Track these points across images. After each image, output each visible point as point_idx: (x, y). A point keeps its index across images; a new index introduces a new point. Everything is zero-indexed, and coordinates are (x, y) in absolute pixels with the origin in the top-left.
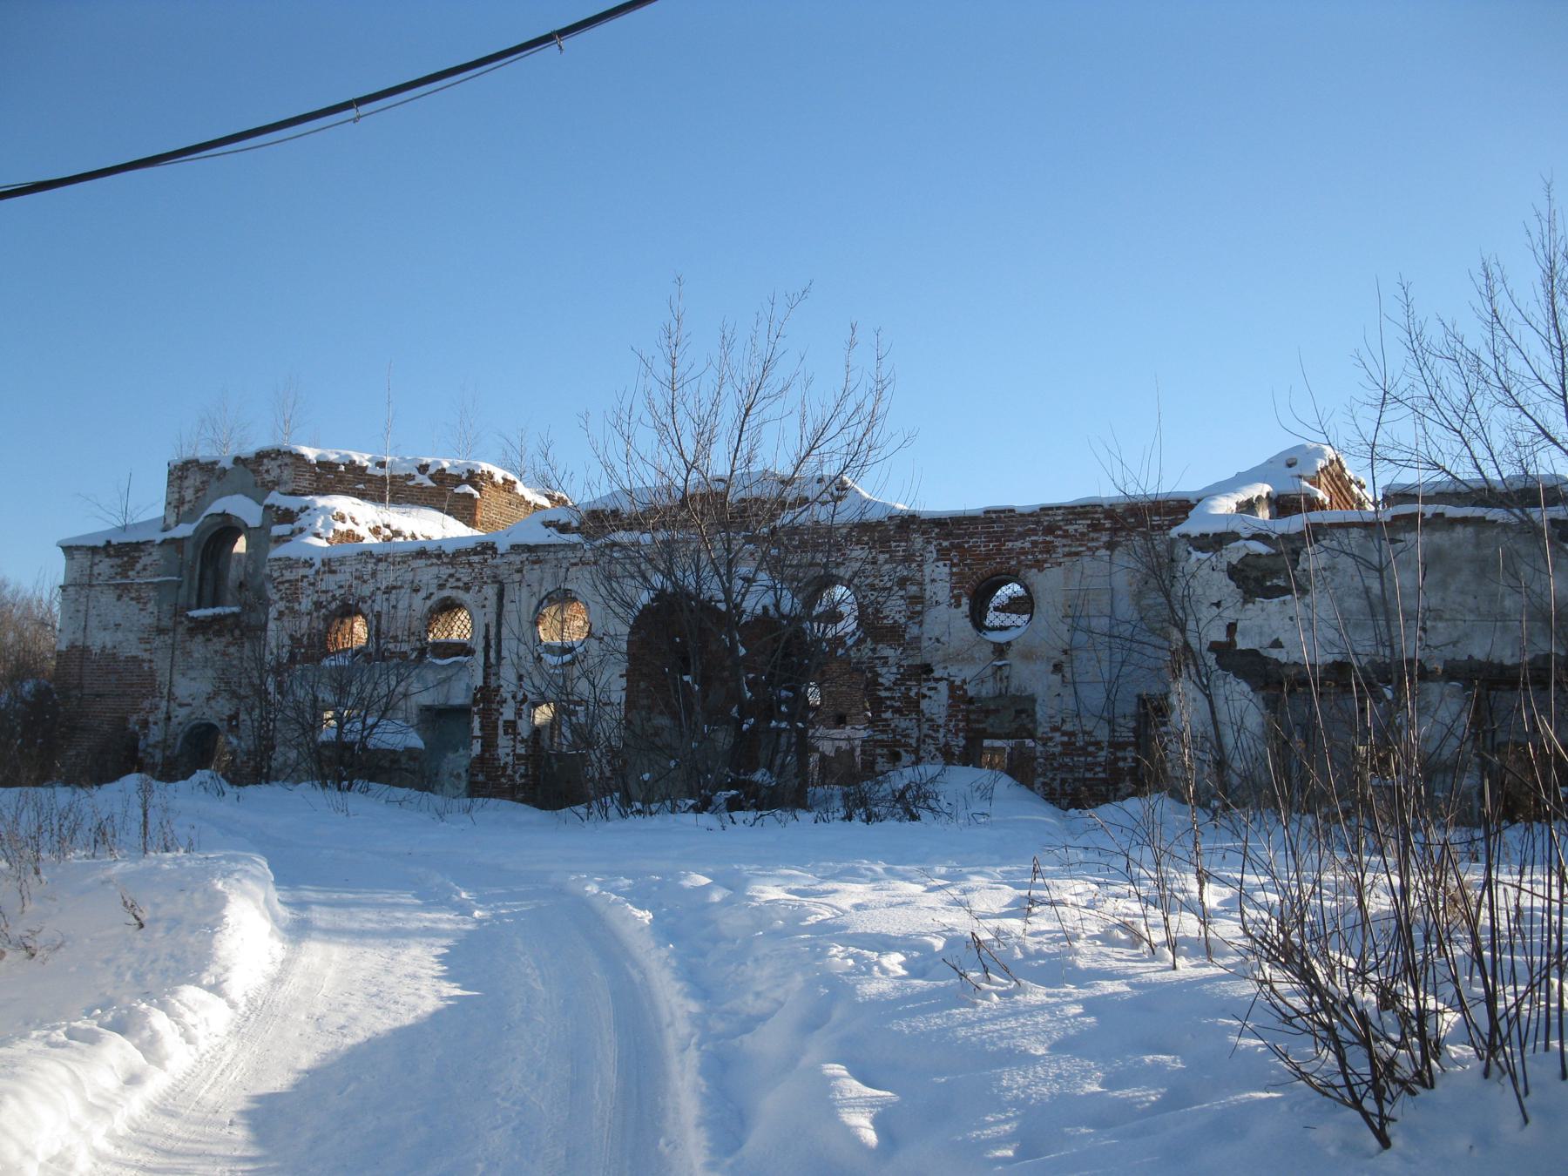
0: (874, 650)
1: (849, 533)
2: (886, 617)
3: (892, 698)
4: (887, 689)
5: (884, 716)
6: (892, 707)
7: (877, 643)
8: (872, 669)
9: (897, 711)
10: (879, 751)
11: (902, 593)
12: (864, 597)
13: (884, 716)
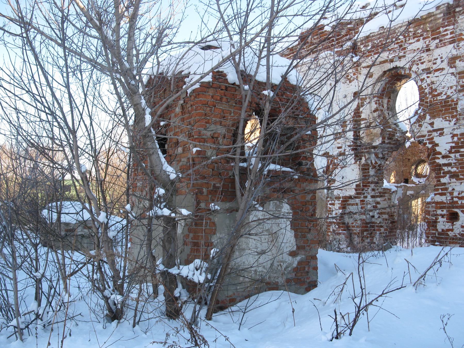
0: (432, 124)
1: (407, 30)
2: (439, 94)
3: (449, 165)
4: (444, 157)
5: (443, 180)
6: (449, 172)
7: (433, 117)
8: (431, 141)
9: (454, 176)
10: (439, 212)
11: (453, 70)
12: (422, 80)
13: (443, 180)
